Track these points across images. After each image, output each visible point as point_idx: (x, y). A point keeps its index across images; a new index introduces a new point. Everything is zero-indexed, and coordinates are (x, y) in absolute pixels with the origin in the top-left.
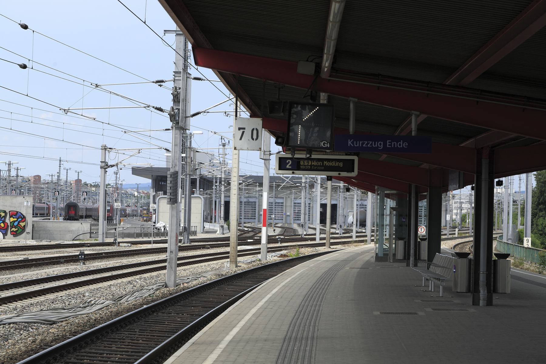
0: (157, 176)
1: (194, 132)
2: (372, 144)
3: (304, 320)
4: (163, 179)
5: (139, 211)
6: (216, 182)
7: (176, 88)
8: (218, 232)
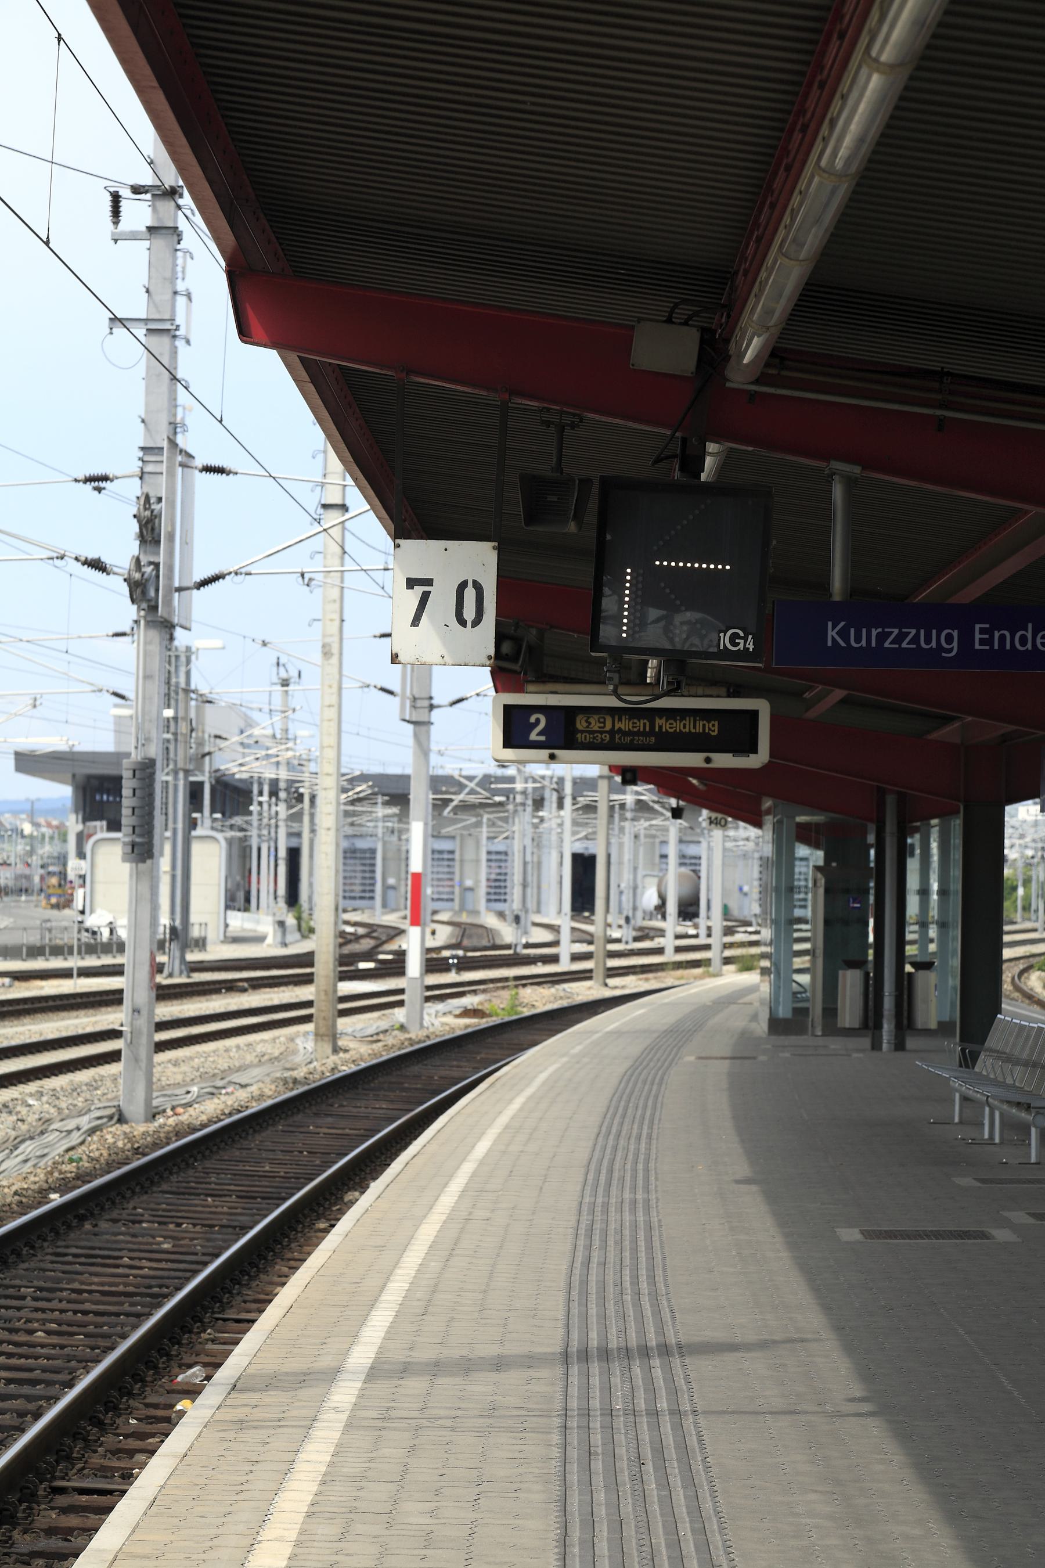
0: (89, 778)
1: (197, 644)
2: (916, 640)
3: (610, 1266)
4: (112, 784)
5: (37, 879)
6: (261, 794)
7: (147, 498)
8: (269, 940)
